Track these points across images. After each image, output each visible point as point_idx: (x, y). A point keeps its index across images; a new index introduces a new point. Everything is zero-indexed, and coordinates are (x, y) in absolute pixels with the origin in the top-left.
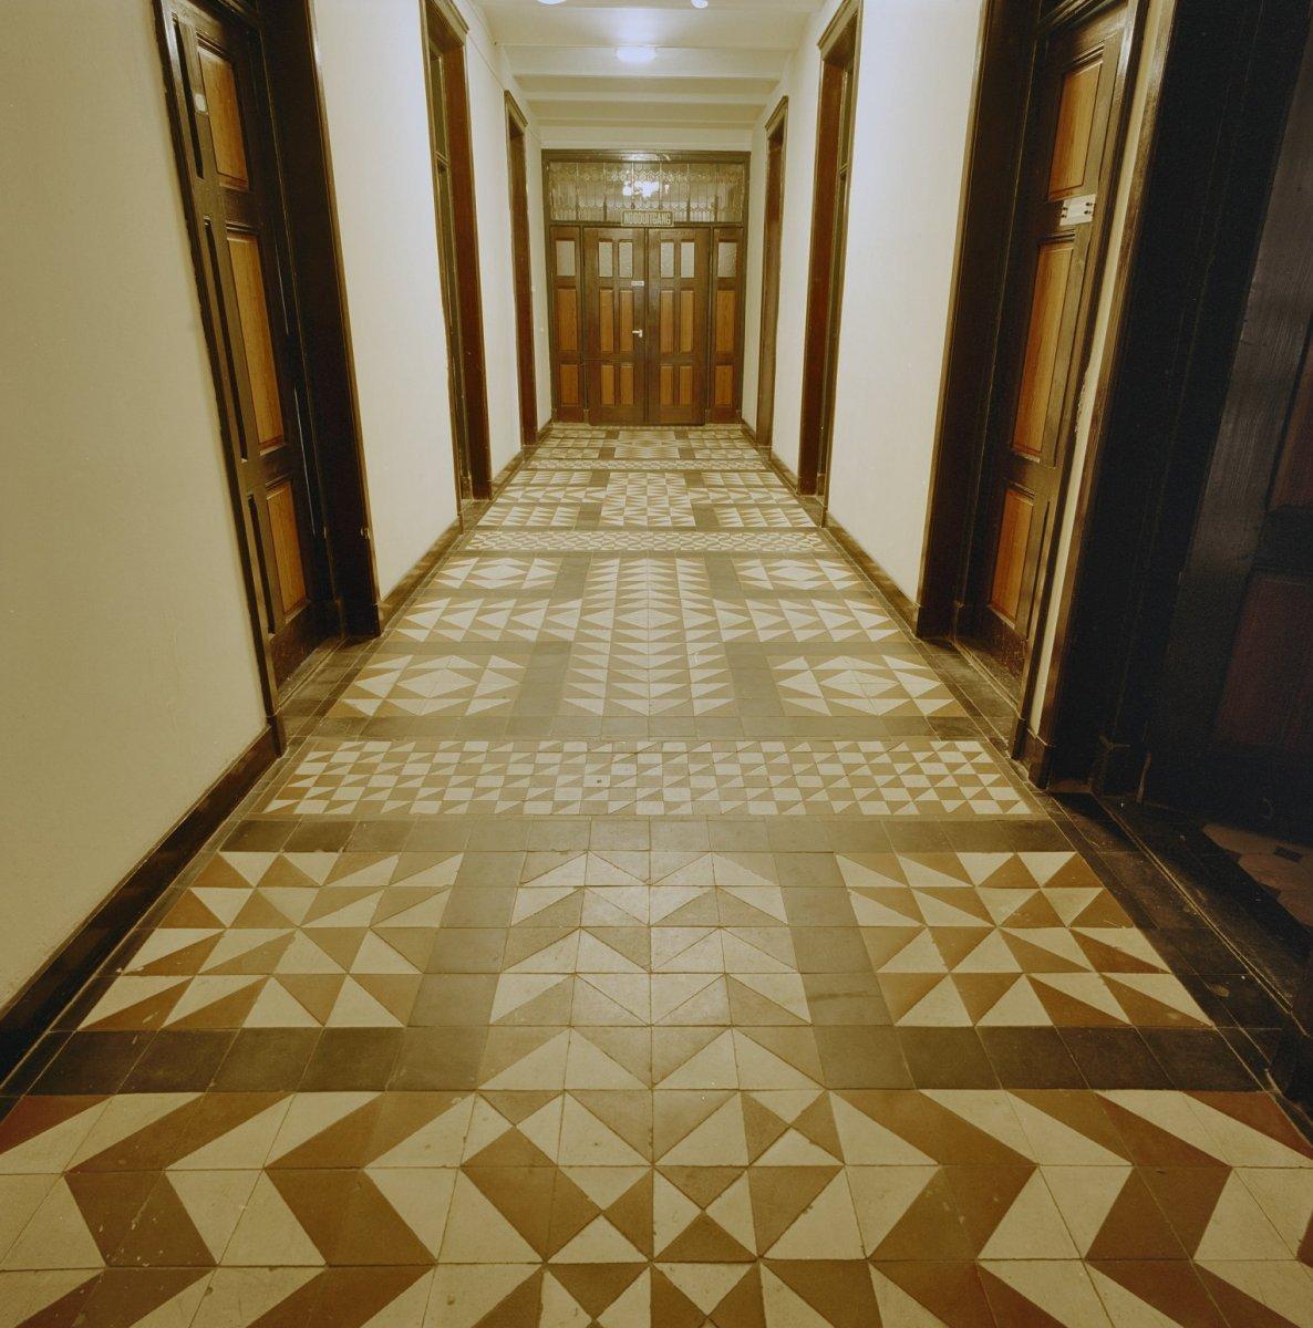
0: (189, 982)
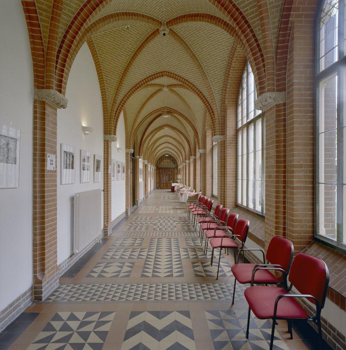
0: (47, 345)
